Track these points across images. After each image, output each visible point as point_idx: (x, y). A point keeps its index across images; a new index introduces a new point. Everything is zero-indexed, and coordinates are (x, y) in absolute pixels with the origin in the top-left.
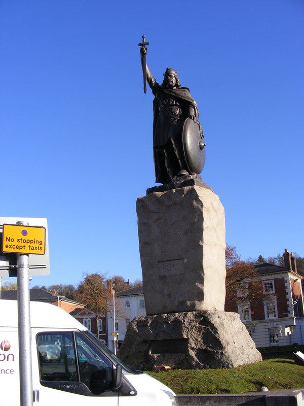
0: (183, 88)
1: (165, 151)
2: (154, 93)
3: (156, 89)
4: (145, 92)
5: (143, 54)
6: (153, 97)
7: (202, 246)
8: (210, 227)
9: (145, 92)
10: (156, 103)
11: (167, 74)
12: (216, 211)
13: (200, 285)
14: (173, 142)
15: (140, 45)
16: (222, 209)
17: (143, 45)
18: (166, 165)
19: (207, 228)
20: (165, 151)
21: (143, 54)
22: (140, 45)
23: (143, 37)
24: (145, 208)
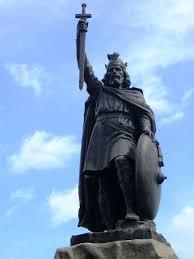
0: (133, 89)
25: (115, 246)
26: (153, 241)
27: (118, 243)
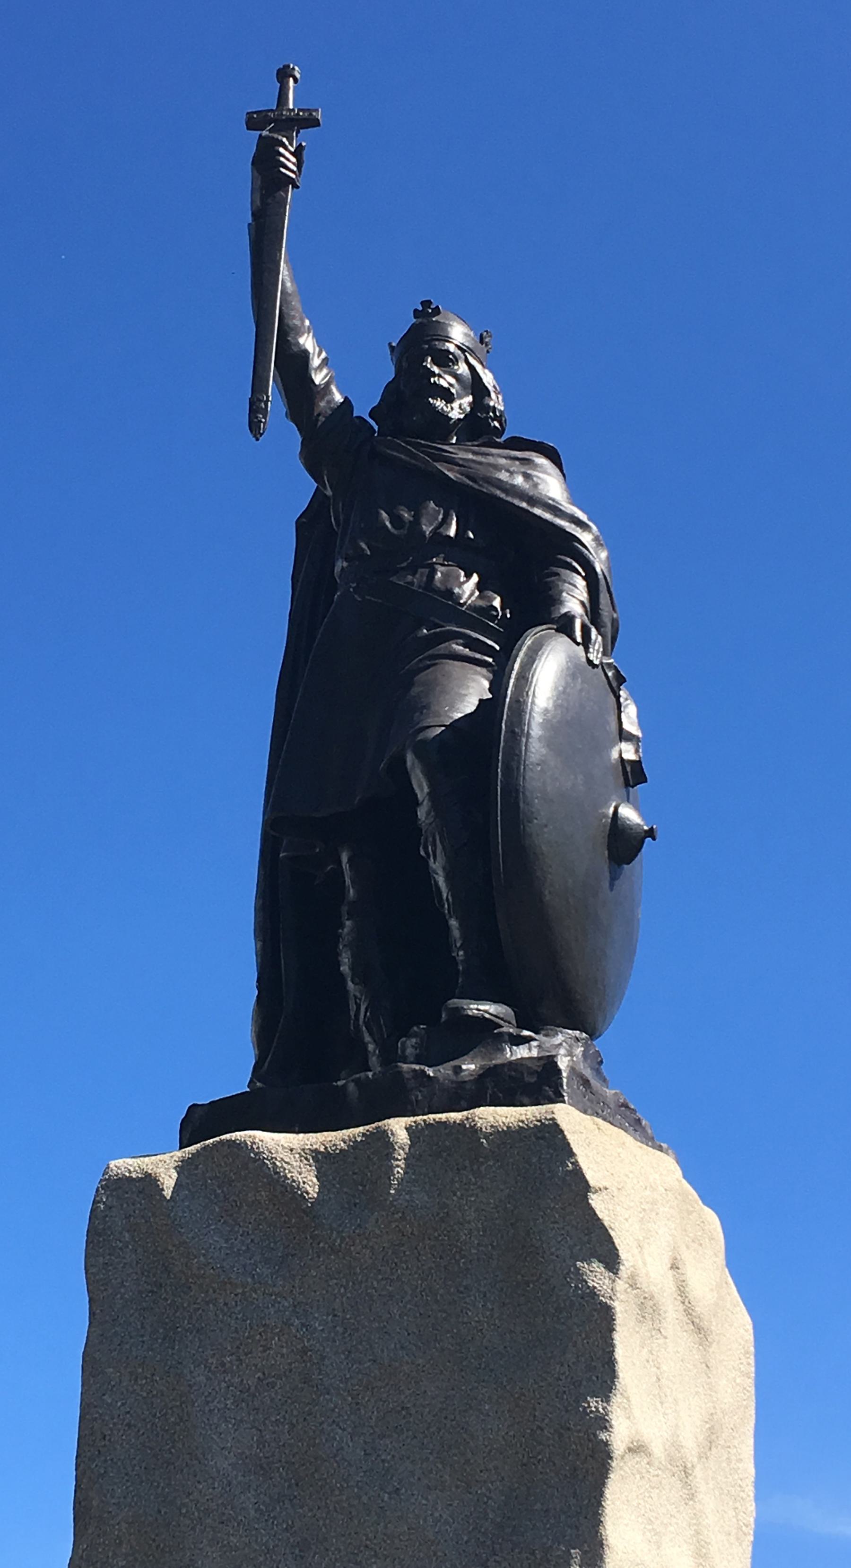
0: (517, 443)
1: (345, 858)
2: (313, 459)
3: (329, 439)
4: (255, 428)
5: (269, 181)
6: (305, 487)
7: (603, 1318)
8: (657, 1449)
9: (255, 428)
10: (315, 533)
11: (421, 342)
12: (699, 1329)
13: (594, 1403)
14: (421, 787)
15: (254, 122)
16: (737, 1327)
17: (273, 125)
18: (345, 969)
19: (636, 1449)
20: (345, 858)
21: (269, 181)
22: (254, 122)
23: (284, 74)
24: (156, 1278)
25: (383, 1139)
26: (567, 1115)
27: (399, 1128)
